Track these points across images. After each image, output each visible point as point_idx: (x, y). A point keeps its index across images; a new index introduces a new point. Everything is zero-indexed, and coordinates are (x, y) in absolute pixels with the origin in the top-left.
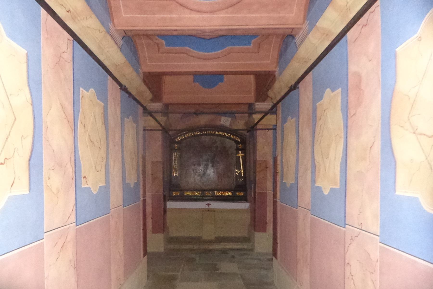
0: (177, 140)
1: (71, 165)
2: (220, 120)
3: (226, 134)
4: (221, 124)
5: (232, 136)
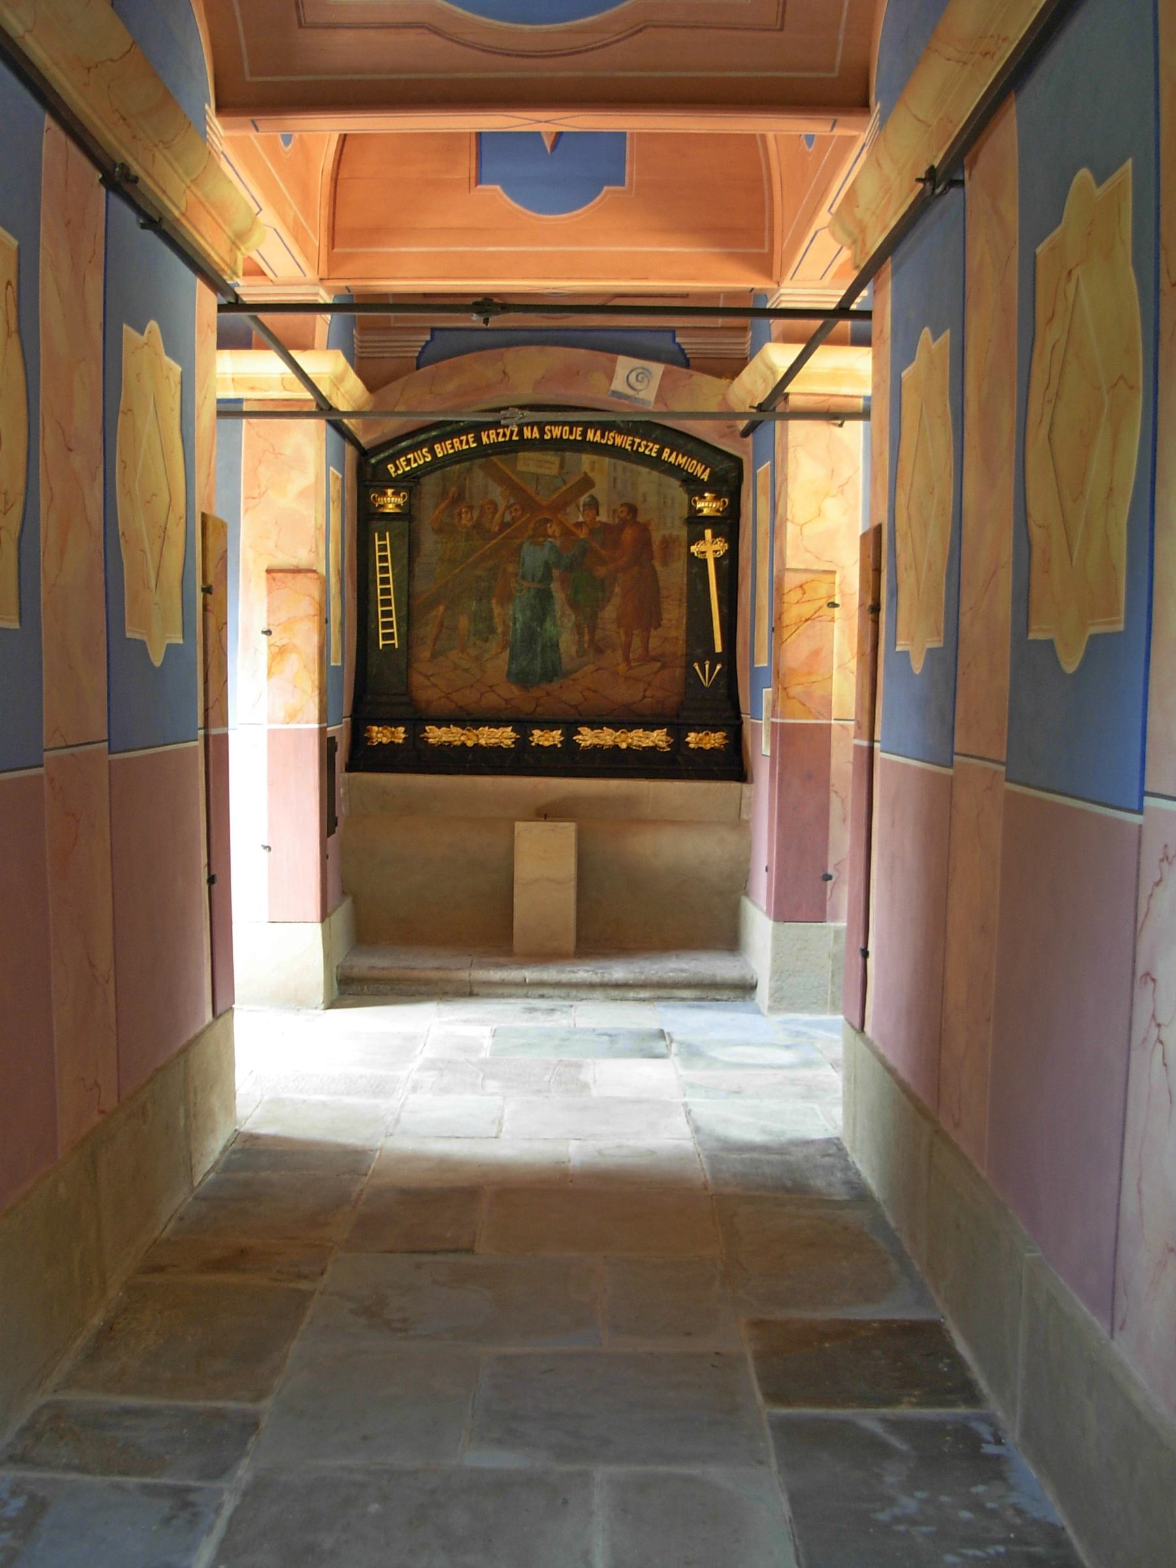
0: (397, 468)
3: (639, 445)
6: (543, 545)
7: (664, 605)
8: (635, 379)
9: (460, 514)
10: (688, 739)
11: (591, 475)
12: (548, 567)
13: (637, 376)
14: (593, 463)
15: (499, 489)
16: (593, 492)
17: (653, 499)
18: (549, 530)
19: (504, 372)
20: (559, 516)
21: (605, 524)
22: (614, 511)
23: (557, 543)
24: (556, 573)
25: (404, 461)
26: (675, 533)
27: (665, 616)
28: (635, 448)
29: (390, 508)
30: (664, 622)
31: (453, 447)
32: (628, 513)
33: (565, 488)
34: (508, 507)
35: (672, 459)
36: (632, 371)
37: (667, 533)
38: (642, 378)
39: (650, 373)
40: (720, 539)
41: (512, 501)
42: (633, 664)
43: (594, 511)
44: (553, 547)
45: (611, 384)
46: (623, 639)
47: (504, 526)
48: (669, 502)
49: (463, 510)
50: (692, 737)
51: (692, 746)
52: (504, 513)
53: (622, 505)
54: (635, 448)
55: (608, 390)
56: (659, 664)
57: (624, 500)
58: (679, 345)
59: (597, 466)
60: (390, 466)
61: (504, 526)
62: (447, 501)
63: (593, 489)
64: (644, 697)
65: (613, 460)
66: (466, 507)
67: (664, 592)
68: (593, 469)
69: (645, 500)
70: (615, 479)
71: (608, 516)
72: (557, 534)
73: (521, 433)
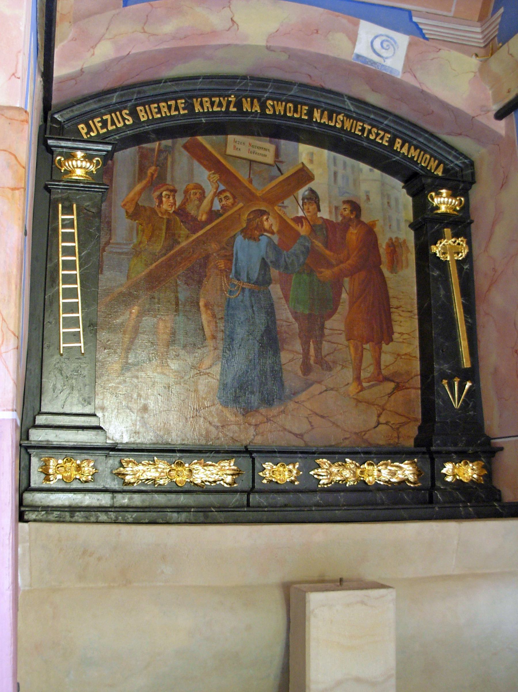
0: (90, 129)
1: (2, 331)
2: (353, 39)
3: (370, 132)
4: (358, 56)
5: (402, 147)
6: (259, 240)
7: (395, 317)
8: (380, 46)
9: (160, 197)
10: (444, 471)
11: (309, 166)
12: (264, 264)
13: (382, 43)
14: (312, 154)
15: (206, 173)
16: (312, 185)
17: (376, 199)
18: (265, 223)
19: (232, 19)
20: (276, 208)
21: (326, 221)
22: (336, 208)
23: (276, 239)
24: (274, 273)
25: (99, 122)
26: (402, 236)
27: (396, 328)
28: (365, 135)
29: (79, 174)
30: (396, 336)
31: (159, 112)
32: (351, 212)
33: (281, 178)
34: (217, 194)
35: (404, 150)
36: (376, 37)
37: (394, 237)
38: (388, 46)
39: (395, 43)
40: (462, 238)
41: (222, 187)
42: (365, 385)
43: (315, 206)
44: (270, 241)
45: (354, 47)
46: (353, 355)
47: (212, 215)
48: (393, 203)
49: (164, 193)
50: (448, 468)
51: (449, 479)
52: (212, 202)
53: (345, 202)
54: (365, 135)
55: (352, 53)
56: (392, 385)
57: (346, 197)
58: (416, 24)
59: (315, 158)
60: (81, 126)
61: (212, 215)
62: (144, 182)
63: (313, 182)
64: (379, 423)
65: (333, 154)
66: (167, 190)
67: (394, 302)
68: (311, 161)
69: (368, 199)
70: (335, 174)
71: (330, 212)
72: (275, 229)
73: (239, 104)
